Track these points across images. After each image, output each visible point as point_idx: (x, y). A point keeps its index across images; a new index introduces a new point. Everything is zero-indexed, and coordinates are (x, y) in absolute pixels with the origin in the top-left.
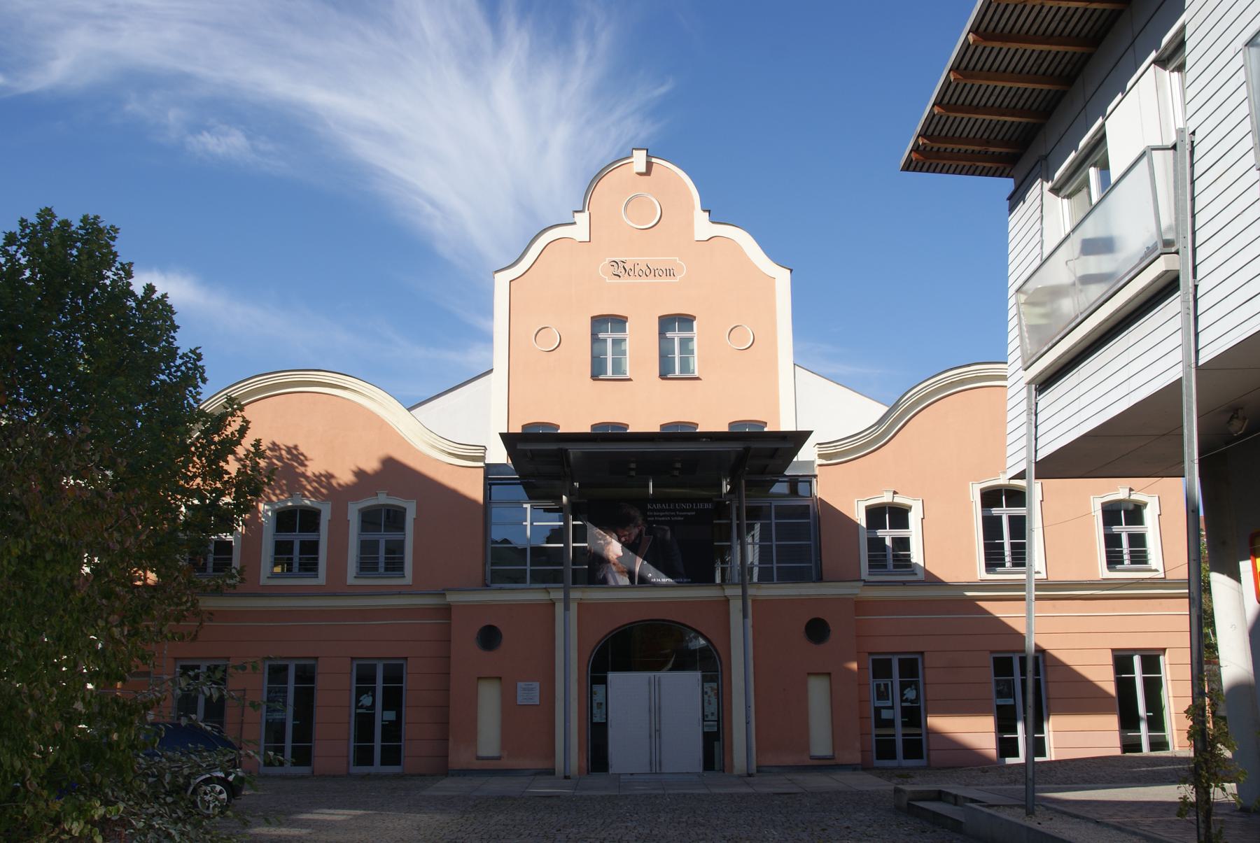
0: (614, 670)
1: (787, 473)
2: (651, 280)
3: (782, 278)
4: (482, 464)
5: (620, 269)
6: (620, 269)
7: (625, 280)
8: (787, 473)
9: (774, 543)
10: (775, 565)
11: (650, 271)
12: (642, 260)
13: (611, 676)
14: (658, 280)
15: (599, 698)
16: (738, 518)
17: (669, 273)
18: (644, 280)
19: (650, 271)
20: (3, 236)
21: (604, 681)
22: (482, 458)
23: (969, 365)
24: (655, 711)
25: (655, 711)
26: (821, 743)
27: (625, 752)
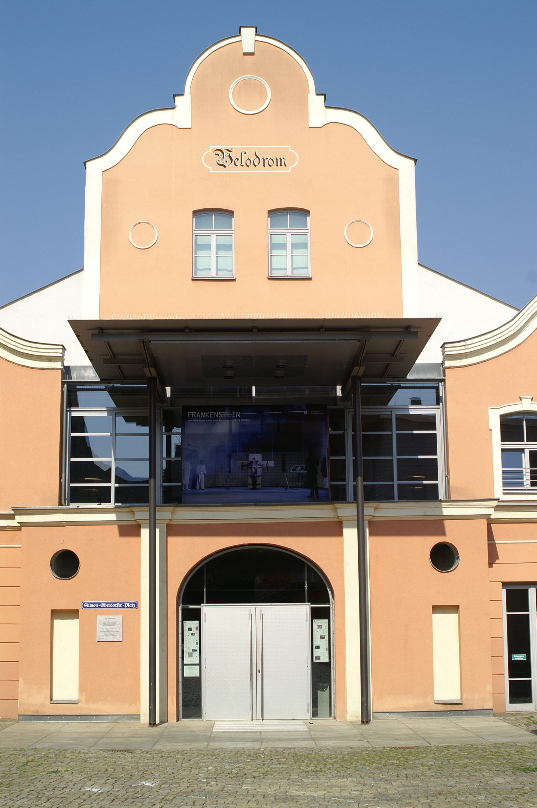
0: (213, 599)
1: (409, 377)
2: (260, 170)
3: (406, 168)
4: (59, 365)
5: (225, 158)
6: (225, 158)
7: (231, 170)
8: (409, 377)
9: (395, 457)
10: (396, 482)
11: (258, 161)
12: (251, 148)
13: (210, 612)
14: (267, 171)
15: (191, 642)
16: (354, 429)
17: (280, 162)
18: (252, 170)
19: (258, 161)
20: (410, 400)
21: (196, 615)
22: (61, 359)
23: (53, 369)
24: (257, 648)
25: (257, 648)
26: (447, 686)
27: (224, 713)
